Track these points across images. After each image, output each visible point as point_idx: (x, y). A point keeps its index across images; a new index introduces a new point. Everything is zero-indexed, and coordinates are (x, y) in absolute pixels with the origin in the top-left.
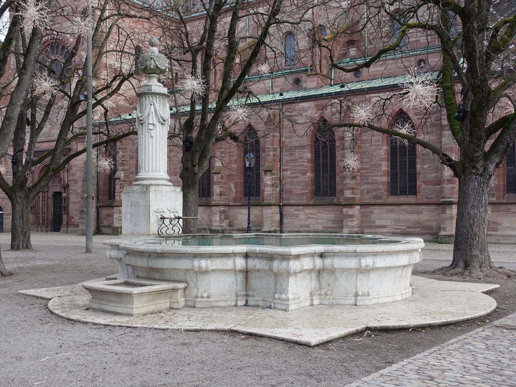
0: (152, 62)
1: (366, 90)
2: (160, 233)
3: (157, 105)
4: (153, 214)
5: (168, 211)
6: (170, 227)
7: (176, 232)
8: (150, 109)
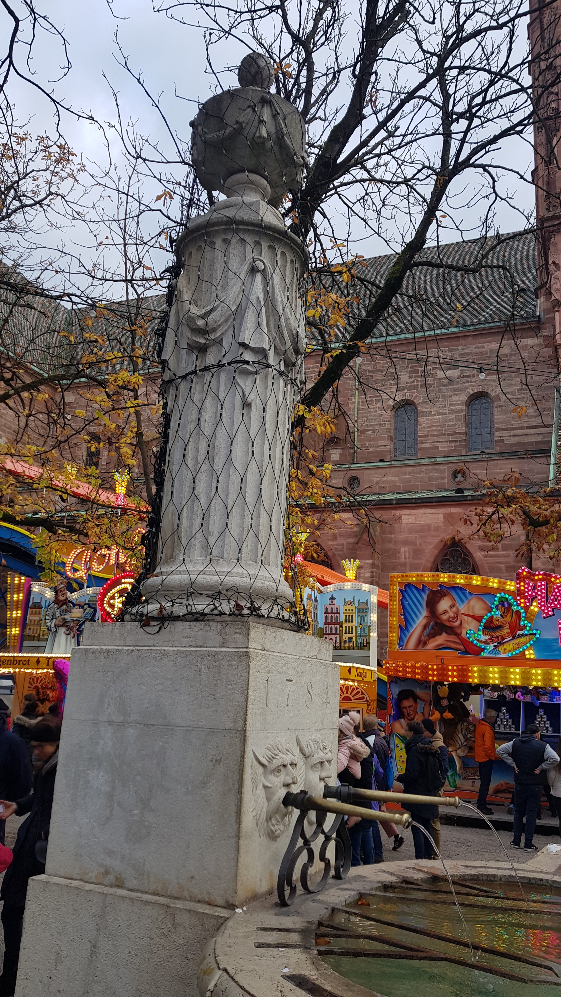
1: (394, 503)
4: (254, 780)
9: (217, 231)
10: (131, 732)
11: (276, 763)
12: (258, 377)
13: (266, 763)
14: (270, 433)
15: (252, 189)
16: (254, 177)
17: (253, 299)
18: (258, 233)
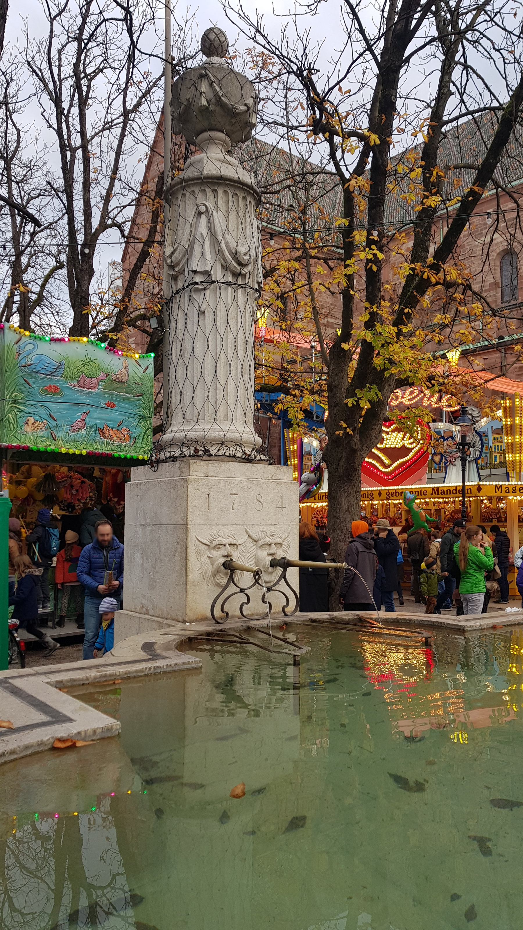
0: (204, 87)
2: (218, 613)
3: (218, 218)
4: (198, 552)
5: (250, 544)
6: (256, 593)
7: (277, 608)
8: (195, 227)
9: (177, 189)
10: (148, 529)
11: (215, 543)
12: (207, 292)
13: (208, 543)
14: (221, 330)
15: (212, 143)
16: (213, 134)
17: (198, 236)
18: (202, 183)
